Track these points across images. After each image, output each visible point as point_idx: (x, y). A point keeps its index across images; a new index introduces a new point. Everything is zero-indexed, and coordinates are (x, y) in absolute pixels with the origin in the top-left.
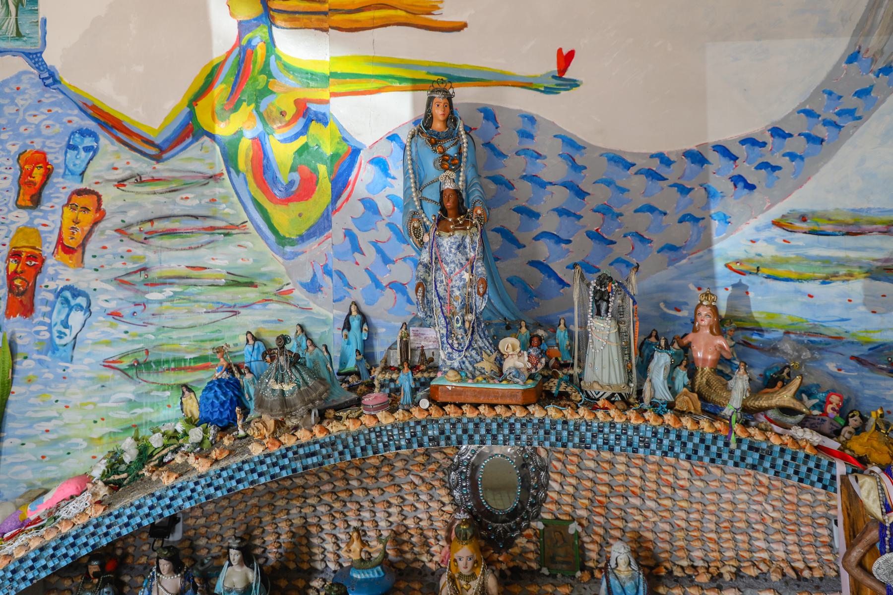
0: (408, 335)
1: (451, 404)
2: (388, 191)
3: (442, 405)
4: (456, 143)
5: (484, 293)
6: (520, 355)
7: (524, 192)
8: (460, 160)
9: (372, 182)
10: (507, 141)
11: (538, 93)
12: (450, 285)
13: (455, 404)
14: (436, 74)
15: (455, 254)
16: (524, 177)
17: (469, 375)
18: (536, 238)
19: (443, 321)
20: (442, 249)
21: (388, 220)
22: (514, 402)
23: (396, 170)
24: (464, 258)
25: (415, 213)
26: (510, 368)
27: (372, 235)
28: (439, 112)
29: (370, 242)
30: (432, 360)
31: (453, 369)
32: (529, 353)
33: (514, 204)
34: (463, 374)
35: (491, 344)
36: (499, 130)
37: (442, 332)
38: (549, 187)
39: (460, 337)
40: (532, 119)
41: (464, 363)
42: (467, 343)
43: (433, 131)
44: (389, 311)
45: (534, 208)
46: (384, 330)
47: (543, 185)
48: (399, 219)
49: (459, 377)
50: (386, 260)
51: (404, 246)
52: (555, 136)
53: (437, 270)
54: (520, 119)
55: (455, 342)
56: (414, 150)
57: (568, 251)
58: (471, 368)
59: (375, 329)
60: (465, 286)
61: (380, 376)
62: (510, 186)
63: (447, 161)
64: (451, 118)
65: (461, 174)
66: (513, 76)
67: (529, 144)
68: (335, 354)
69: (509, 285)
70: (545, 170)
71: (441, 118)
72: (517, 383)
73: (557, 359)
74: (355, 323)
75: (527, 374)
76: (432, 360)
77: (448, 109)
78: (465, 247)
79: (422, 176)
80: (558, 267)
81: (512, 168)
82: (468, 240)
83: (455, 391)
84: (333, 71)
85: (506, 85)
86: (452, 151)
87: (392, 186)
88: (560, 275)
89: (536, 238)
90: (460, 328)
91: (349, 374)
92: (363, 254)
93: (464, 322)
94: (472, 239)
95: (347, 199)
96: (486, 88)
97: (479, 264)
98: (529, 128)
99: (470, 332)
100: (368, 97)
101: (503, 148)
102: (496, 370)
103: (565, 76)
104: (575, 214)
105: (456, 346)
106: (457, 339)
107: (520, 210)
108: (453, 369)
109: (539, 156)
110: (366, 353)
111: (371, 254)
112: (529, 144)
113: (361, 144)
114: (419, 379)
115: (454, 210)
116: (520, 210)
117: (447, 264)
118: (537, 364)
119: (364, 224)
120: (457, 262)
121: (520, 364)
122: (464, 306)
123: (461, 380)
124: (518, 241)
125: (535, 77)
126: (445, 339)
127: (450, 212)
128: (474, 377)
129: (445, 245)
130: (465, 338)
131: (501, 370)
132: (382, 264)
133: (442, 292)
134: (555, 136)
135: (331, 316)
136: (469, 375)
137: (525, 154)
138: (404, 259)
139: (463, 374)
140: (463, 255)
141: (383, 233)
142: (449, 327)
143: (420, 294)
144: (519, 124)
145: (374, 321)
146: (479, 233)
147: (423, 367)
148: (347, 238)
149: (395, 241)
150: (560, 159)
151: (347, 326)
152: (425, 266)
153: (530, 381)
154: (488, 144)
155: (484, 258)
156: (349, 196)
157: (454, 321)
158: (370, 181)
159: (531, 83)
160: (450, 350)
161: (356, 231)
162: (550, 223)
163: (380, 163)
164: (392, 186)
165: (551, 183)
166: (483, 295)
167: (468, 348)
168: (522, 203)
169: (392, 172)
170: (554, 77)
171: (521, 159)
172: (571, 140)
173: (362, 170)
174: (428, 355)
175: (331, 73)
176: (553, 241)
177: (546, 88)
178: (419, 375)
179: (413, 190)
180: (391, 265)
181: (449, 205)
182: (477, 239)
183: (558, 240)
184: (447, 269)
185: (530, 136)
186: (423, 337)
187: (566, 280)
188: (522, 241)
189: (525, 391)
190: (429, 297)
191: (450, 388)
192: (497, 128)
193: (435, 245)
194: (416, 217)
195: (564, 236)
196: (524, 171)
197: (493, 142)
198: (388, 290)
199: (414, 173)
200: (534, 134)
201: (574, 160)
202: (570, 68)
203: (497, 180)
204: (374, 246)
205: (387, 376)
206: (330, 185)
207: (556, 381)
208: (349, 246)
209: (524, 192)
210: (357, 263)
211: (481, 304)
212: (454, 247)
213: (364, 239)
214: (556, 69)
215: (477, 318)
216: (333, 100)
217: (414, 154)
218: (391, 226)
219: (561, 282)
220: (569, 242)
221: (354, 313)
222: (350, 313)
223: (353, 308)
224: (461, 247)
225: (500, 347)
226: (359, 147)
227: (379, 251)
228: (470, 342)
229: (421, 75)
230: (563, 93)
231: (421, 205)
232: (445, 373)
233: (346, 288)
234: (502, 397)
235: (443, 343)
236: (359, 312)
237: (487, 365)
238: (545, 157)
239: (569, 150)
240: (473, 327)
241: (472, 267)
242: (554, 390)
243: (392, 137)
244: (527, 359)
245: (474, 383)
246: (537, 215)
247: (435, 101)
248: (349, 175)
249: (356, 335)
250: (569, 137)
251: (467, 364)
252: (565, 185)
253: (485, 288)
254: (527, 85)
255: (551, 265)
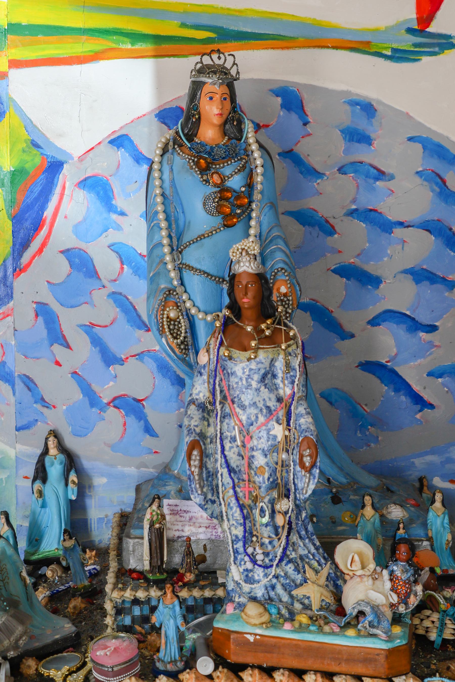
0: (163, 517)
1: (253, 667)
2: (113, 236)
3: (237, 669)
4: (244, 167)
5: (313, 465)
6: (375, 576)
7: (353, 239)
8: (250, 195)
9: (85, 219)
10: (323, 146)
11: (381, 61)
12: (249, 446)
13: (260, 668)
14: (198, 27)
15: (258, 390)
16: (352, 213)
17: (284, 611)
18: (374, 322)
19: (237, 514)
20: (233, 380)
21: (111, 288)
22: (371, 672)
23: (132, 200)
24: (273, 397)
25: (170, 292)
26: (358, 603)
27: (84, 314)
28: (212, 111)
29: (80, 326)
30: (203, 559)
31: (254, 599)
32: (392, 573)
33: (334, 261)
34: (274, 611)
35: (317, 549)
36: (309, 129)
37: (234, 532)
38: (398, 232)
39: (267, 541)
40: (368, 109)
41: (273, 587)
42: (279, 552)
43: (202, 145)
44: (113, 447)
45: (371, 268)
46: (105, 480)
47: (387, 227)
48: (139, 293)
49: (266, 618)
50: (109, 359)
51: (141, 333)
52: (410, 139)
53: (224, 417)
54: (348, 108)
55: (259, 551)
56: (166, 176)
57: (431, 344)
58: (285, 598)
59: (90, 478)
60: (274, 449)
61: (115, 595)
62: (328, 229)
63: (227, 199)
64: (233, 122)
65: (253, 223)
66: (336, 29)
67: (363, 154)
68: (20, 522)
69: (324, 403)
70: (391, 200)
71: (217, 121)
72: (374, 636)
73: (432, 570)
74: (55, 469)
75: (389, 614)
76: (203, 559)
77: (228, 104)
78: (274, 376)
79: (181, 223)
80: (412, 373)
81: (332, 196)
82: (280, 365)
83: (262, 645)
84: (13, 22)
85: (321, 45)
86: (236, 182)
87: (119, 228)
88: (416, 387)
89: (374, 322)
90: (267, 525)
91: (48, 561)
92: (69, 347)
93: (273, 512)
94: (283, 361)
95: (40, 251)
96: (286, 52)
97: (301, 410)
98: (362, 124)
99: (285, 533)
100: (76, 68)
101: (315, 161)
102: (330, 599)
103: (432, 29)
104: (444, 279)
105: (260, 557)
106: (262, 545)
107: (345, 271)
108: (254, 599)
109: (381, 174)
110: (76, 524)
111: (82, 352)
112: (363, 154)
113: (64, 152)
114: (185, 600)
115: (253, 311)
116: (345, 271)
117: (243, 407)
118: (407, 596)
119: (69, 294)
120: (261, 405)
121: (379, 598)
122: (274, 485)
123: (271, 624)
124: (340, 326)
125: (376, 32)
126: (239, 545)
127: (247, 313)
128: (292, 617)
129: (239, 373)
130: (276, 543)
131: (338, 600)
132: (100, 364)
133: (234, 460)
134: (410, 139)
135: (12, 453)
136: (284, 611)
137: (355, 172)
138: (139, 356)
139: (274, 611)
140: (271, 391)
141: (102, 310)
142: (248, 524)
143: (195, 462)
144: (345, 116)
145: (86, 464)
146: (299, 351)
147: (189, 577)
148: (40, 319)
149: (123, 325)
150: (418, 180)
151: (41, 474)
152: (202, 407)
153: (397, 630)
154: (289, 154)
155: (306, 397)
156: (44, 245)
157: (257, 512)
158: (80, 218)
159: (369, 43)
160: (249, 565)
161: (55, 306)
162: (398, 294)
163: (97, 187)
164: (119, 228)
165: (401, 224)
166: (309, 470)
167: (281, 560)
168: (350, 259)
169: (119, 202)
170: (410, 31)
171: (348, 182)
172: (439, 146)
173: (66, 199)
174: (197, 550)
175: (10, 25)
176: (404, 326)
177: (395, 50)
178: (184, 594)
179: (166, 250)
180: (117, 367)
181: (246, 301)
182: (296, 362)
183: (414, 325)
184: (244, 418)
185: (364, 139)
186: (187, 516)
187: (426, 396)
188: (348, 327)
189: (390, 652)
190: (210, 465)
191: (251, 638)
192: (305, 124)
193: (220, 370)
194: (172, 299)
195: (423, 317)
196: (354, 201)
197: (298, 149)
198: (111, 410)
199: (167, 219)
200: (373, 136)
201: (444, 182)
202: (439, 14)
203: (305, 218)
204: (87, 333)
205: (128, 594)
206: (9, 225)
207: (435, 617)
208: (44, 333)
209: (353, 239)
210: (58, 363)
211: (307, 485)
212: (256, 377)
213: (70, 321)
214: (414, 16)
215: (297, 506)
216: (14, 73)
217: (167, 184)
218: (118, 298)
219: (418, 400)
220: (432, 328)
221: (53, 451)
222: (46, 451)
223: (52, 443)
224: (268, 377)
225: (338, 558)
226: (60, 158)
227: (96, 342)
228: (285, 549)
229: (171, 28)
230: (425, 59)
231: (181, 279)
232: (241, 607)
233: (38, 406)
234: (348, 661)
235: (236, 552)
236: (62, 448)
237: (315, 593)
238: (392, 177)
239: (435, 164)
240: (290, 523)
241: (289, 415)
242: (433, 636)
243: (119, 141)
244: (388, 585)
245: (295, 631)
246: (376, 281)
247: (206, 89)
248: (43, 208)
249: (57, 491)
250: (436, 139)
251: (279, 589)
252: (428, 226)
253: (314, 457)
254: (360, 46)
255: (400, 370)
